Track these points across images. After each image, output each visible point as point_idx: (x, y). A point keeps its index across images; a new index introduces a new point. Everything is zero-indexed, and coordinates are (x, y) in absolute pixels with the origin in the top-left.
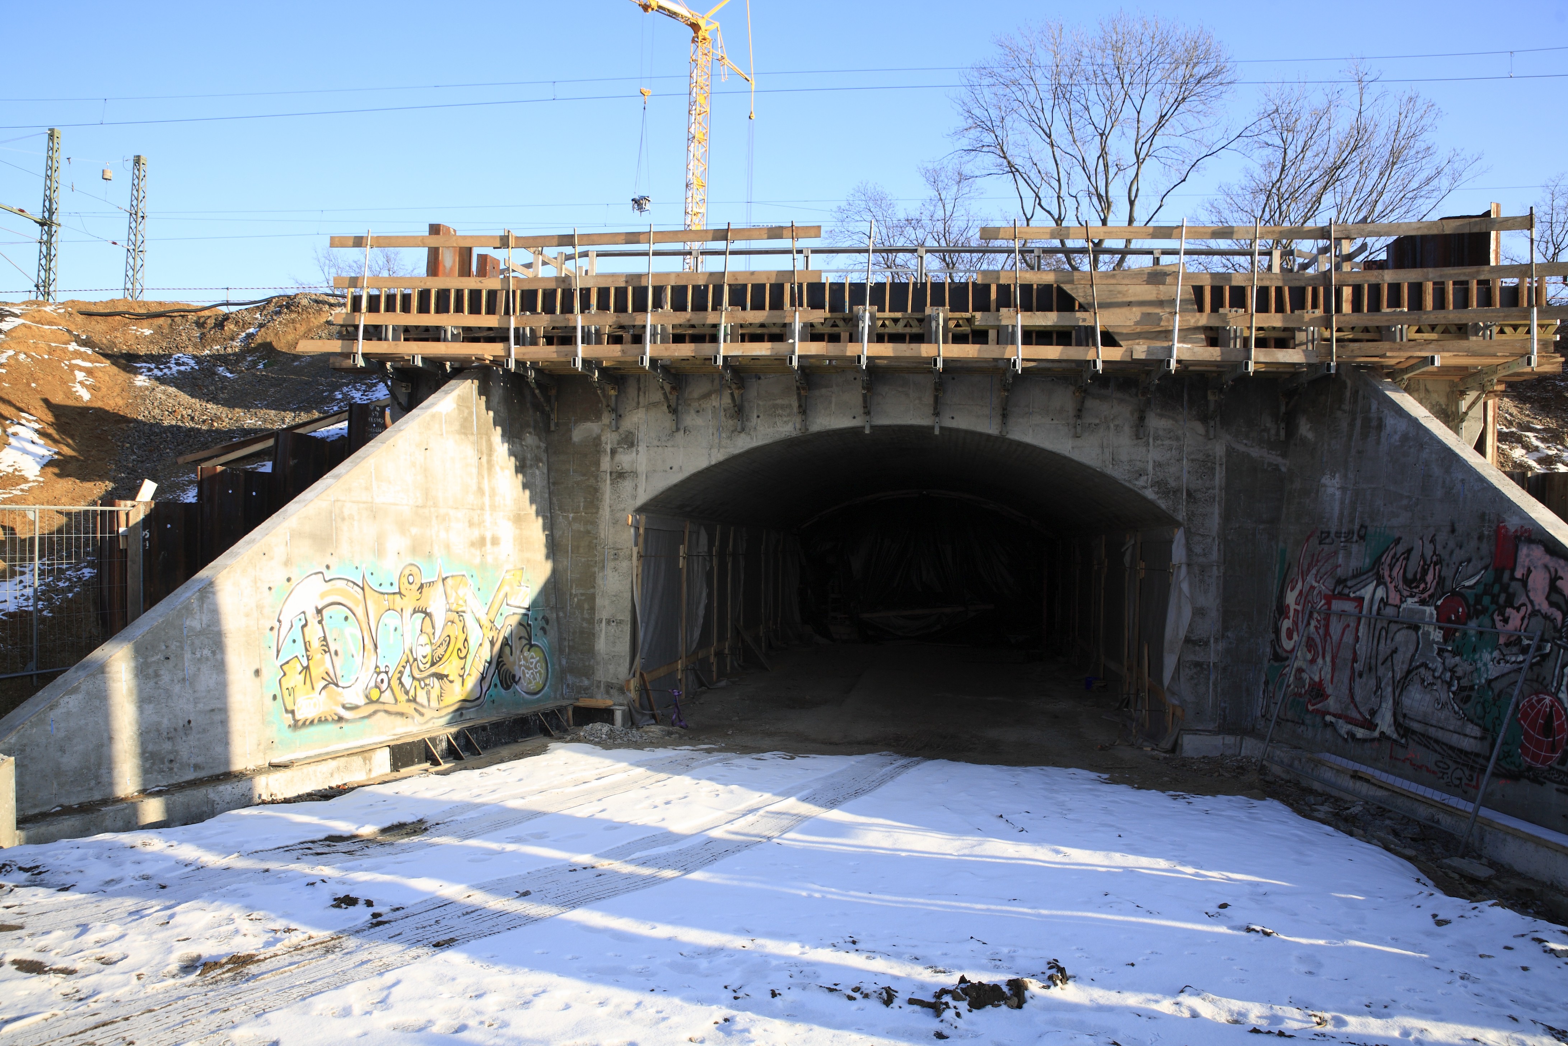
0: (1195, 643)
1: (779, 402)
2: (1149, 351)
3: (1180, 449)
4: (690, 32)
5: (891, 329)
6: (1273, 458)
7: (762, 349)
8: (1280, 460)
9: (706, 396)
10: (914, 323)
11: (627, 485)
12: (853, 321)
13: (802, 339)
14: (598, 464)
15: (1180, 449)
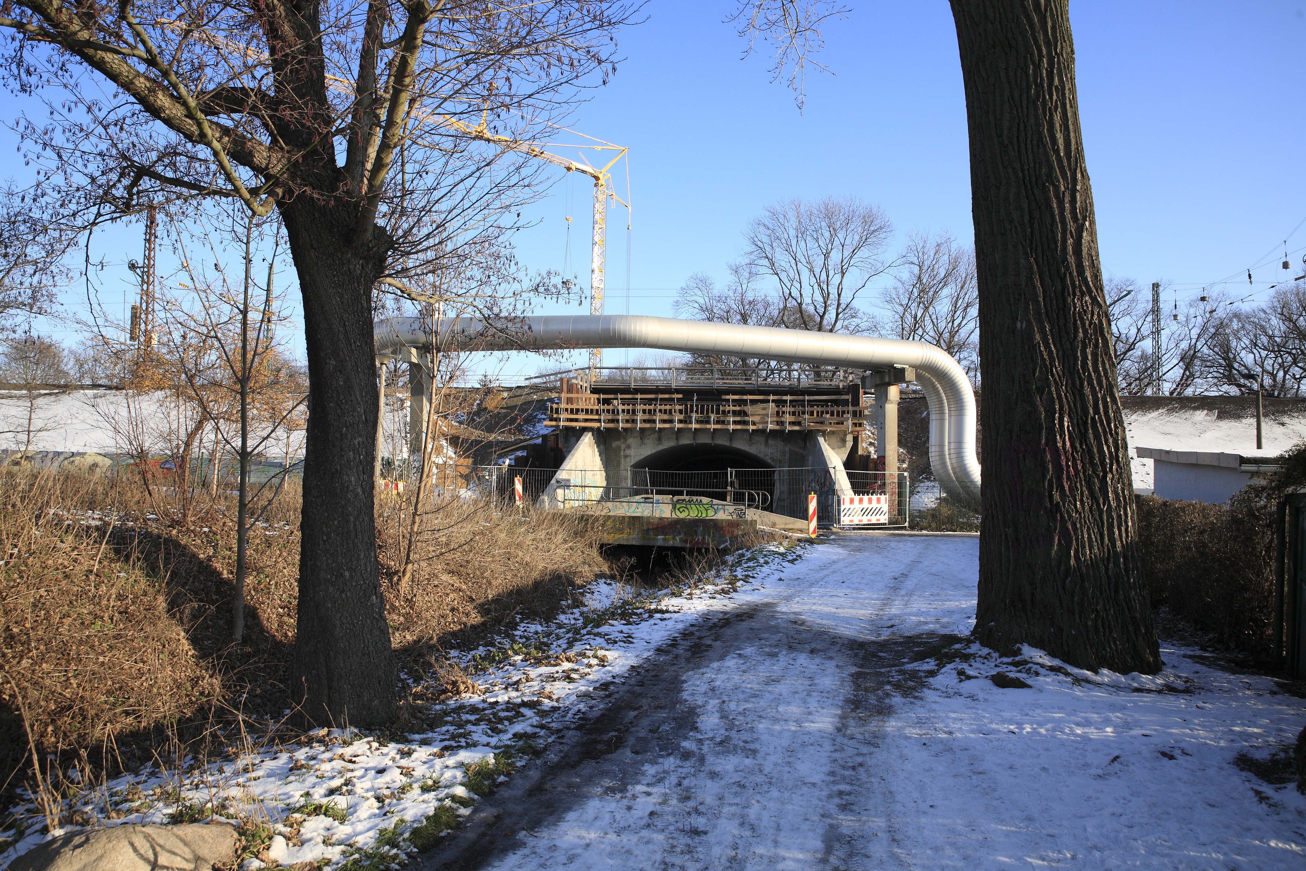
4: (594, 181)
7: (667, 426)
11: (628, 459)
12: (691, 417)
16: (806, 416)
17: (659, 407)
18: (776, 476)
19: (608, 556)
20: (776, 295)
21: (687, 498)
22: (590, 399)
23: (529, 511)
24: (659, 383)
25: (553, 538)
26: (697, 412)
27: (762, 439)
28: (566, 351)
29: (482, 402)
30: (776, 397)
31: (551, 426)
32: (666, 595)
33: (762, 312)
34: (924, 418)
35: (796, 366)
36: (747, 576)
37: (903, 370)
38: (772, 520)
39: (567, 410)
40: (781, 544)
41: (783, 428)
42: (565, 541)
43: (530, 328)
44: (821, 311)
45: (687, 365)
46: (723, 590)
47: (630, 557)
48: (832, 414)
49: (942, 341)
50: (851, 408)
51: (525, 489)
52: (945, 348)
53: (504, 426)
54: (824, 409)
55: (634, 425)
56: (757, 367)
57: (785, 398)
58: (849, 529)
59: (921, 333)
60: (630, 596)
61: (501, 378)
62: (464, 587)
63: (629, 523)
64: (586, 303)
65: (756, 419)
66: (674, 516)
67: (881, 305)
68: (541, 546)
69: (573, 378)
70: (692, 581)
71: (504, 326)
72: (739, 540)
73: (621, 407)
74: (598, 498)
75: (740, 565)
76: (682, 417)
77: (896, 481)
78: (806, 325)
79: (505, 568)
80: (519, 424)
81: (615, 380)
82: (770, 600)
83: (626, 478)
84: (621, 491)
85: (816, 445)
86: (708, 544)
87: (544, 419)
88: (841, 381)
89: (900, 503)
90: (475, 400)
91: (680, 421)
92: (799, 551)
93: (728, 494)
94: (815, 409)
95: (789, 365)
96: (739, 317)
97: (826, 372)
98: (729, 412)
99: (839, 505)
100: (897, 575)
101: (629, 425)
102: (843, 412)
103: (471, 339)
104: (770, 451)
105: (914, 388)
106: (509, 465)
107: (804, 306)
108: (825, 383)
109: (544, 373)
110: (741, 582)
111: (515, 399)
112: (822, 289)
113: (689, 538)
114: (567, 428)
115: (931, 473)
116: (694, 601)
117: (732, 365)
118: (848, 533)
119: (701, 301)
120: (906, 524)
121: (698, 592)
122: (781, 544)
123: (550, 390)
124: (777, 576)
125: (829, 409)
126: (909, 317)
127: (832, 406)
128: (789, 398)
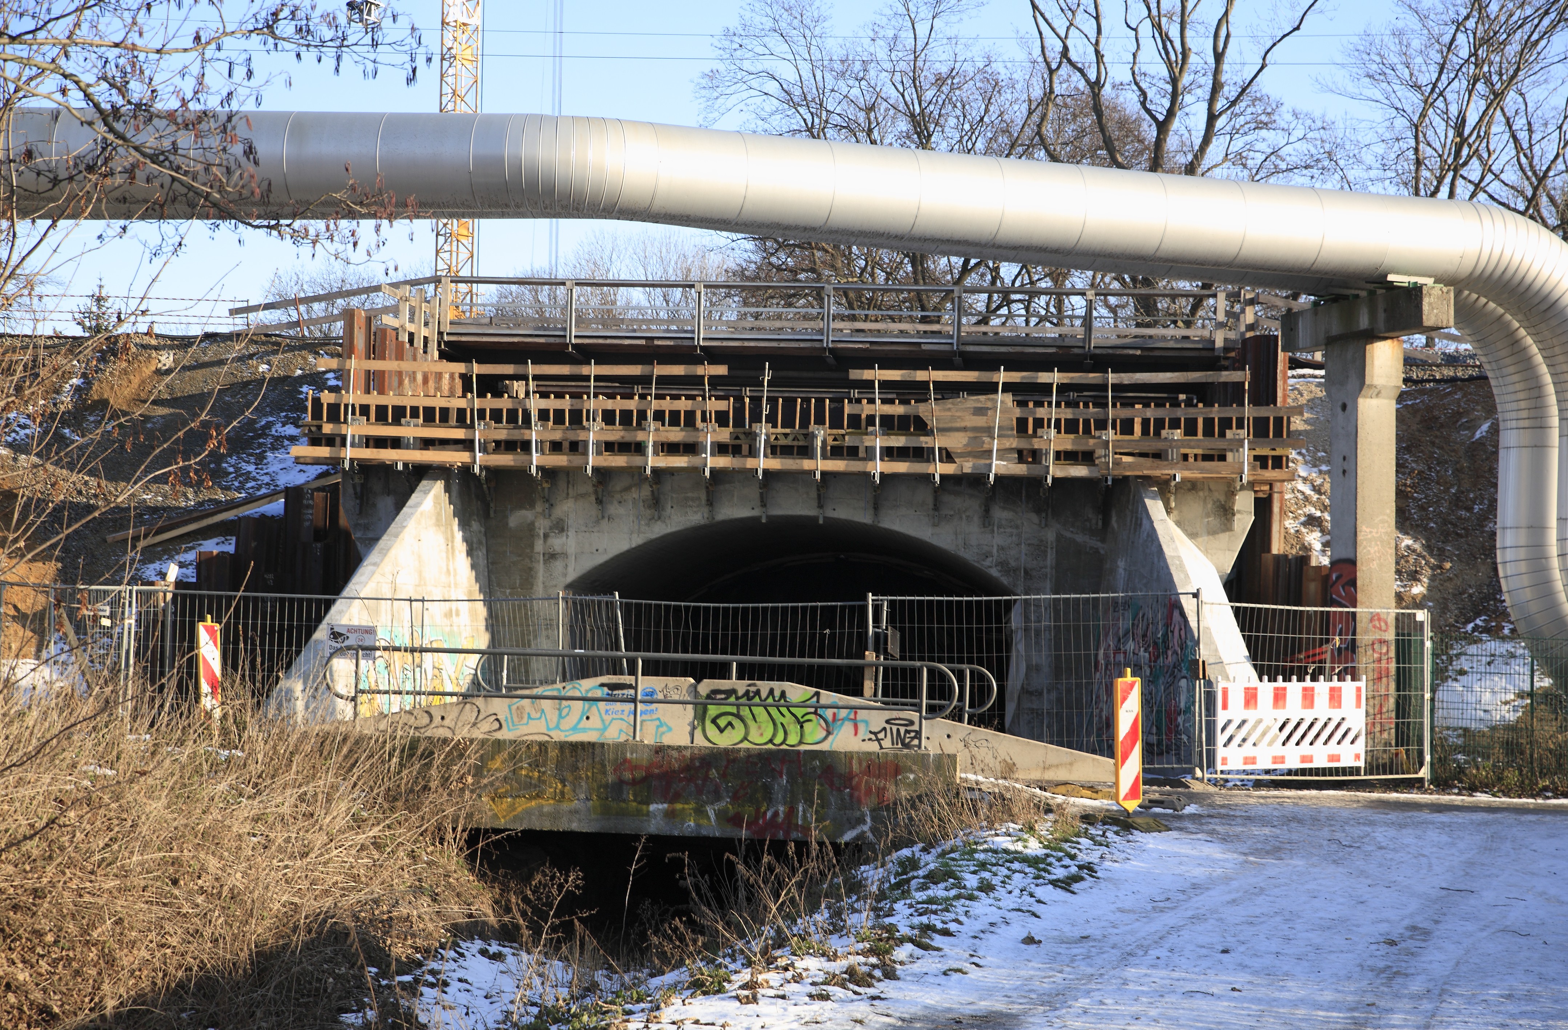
0: (1031, 693)
1: (690, 495)
2: (974, 467)
3: (1019, 535)
5: (783, 442)
6: (1094, 542)
7: (680, 461)
8: (1099, 544)
9: (627, 489)
10: (801, 437)
11: (558, 565)
12: (752, 436)
13: (712, 454)
14: (532, 546)
15: (1019, 535)
16: (1110, 435)
17: (655, 405)
18: (1016, 620)
19: (494, 867)
20: (1021, 56)
21: (741, 686)
22: (439, 376)
23: (242, 727)
24: (655, 330)
25: (319, 812)
26: (772, 419)
27: (972, 504)
28: (366, 226)
29: (88, 383)
30: (1016, 377)
31: (317, 461)
32: (674, 988)
33: (976, 109)
34: (1481, 443)
35: (1079, 279)
36: (927, 929)
37: (1415, 293)
38: (1002, 754)
39: (365, 410)
40: (1031, 829)
41: (1036, 470)
42: (358, 823)
43: (250, 151)
44: (1160, 105)
45: (741, 273)
46: (851, 972)
47: (565, 870)
48: (1191, 429)
49: (1544, 200)
50: (1249, 411)
51: (229, 658)
52: (1553, 221)
53: (166, 459)
54: (1166, 413)
55: (577, 460)
56: (958, 282)
57: (1044, 377)
58: (1244, 785)
59: (1475, 176)
60: (563, 993)
61: (154, 306)
62: (23, 976)
63: (559, 765)
64: (428, 75)
65: (955, 442)
66: (700, 741)
67: (1351, 88)
68: (279, 837)
69: (386, 310)
70: (756, 946)
71: (167, 144)
72: (902, 816)
73: (535, 404)
74: (464, 684)
75: (906, 894)
76: (725, 435)
77: (1390, 635)
78: (1111, 151)
79: (162, 912)
80: (215, 456)
81: (517, 319)
82: (1000, 1006)
83: (551, 625)
84: (538, 666)
85: (1138, 524)
86: (806, 829)
87: (293, 439)
88: (1221, 325)
89: (1402, 707)
90: (66, 376)
91: (721, 449)
92: (1086, 851)
93: (869, 673)
94: (1138, 413)
95: (1058, 277)
96: (903, 125)
97: (1174, 297)
98: (871, 420)
99: (1211, 708)
100: (1396, 932)
101: (560, 460)
102: (1226, 423)
103: (56, 182)
104: (998, 540)
105: (1451, 348)
106: (179, 584)
107: (1107, 91)
108: (1171, 331)
109: (292, 292)
110: (909, 947)
111: (199, 374)
112: (1166, 39)
113: (748, 811)
114: (365, 468)
115: (1504, 615)
116: (764, 1007)
117: (881, 276)
118: (1240, 797)
119: (788, 73)
120: (1424, 772)
121: (773, 977)
122: (1031, 829)
123: (313, 347)
124: (1019, 927)
125: (1182, 413)
126: (1440, 125)
127: (1189, 403)
128: (1055, 377)
